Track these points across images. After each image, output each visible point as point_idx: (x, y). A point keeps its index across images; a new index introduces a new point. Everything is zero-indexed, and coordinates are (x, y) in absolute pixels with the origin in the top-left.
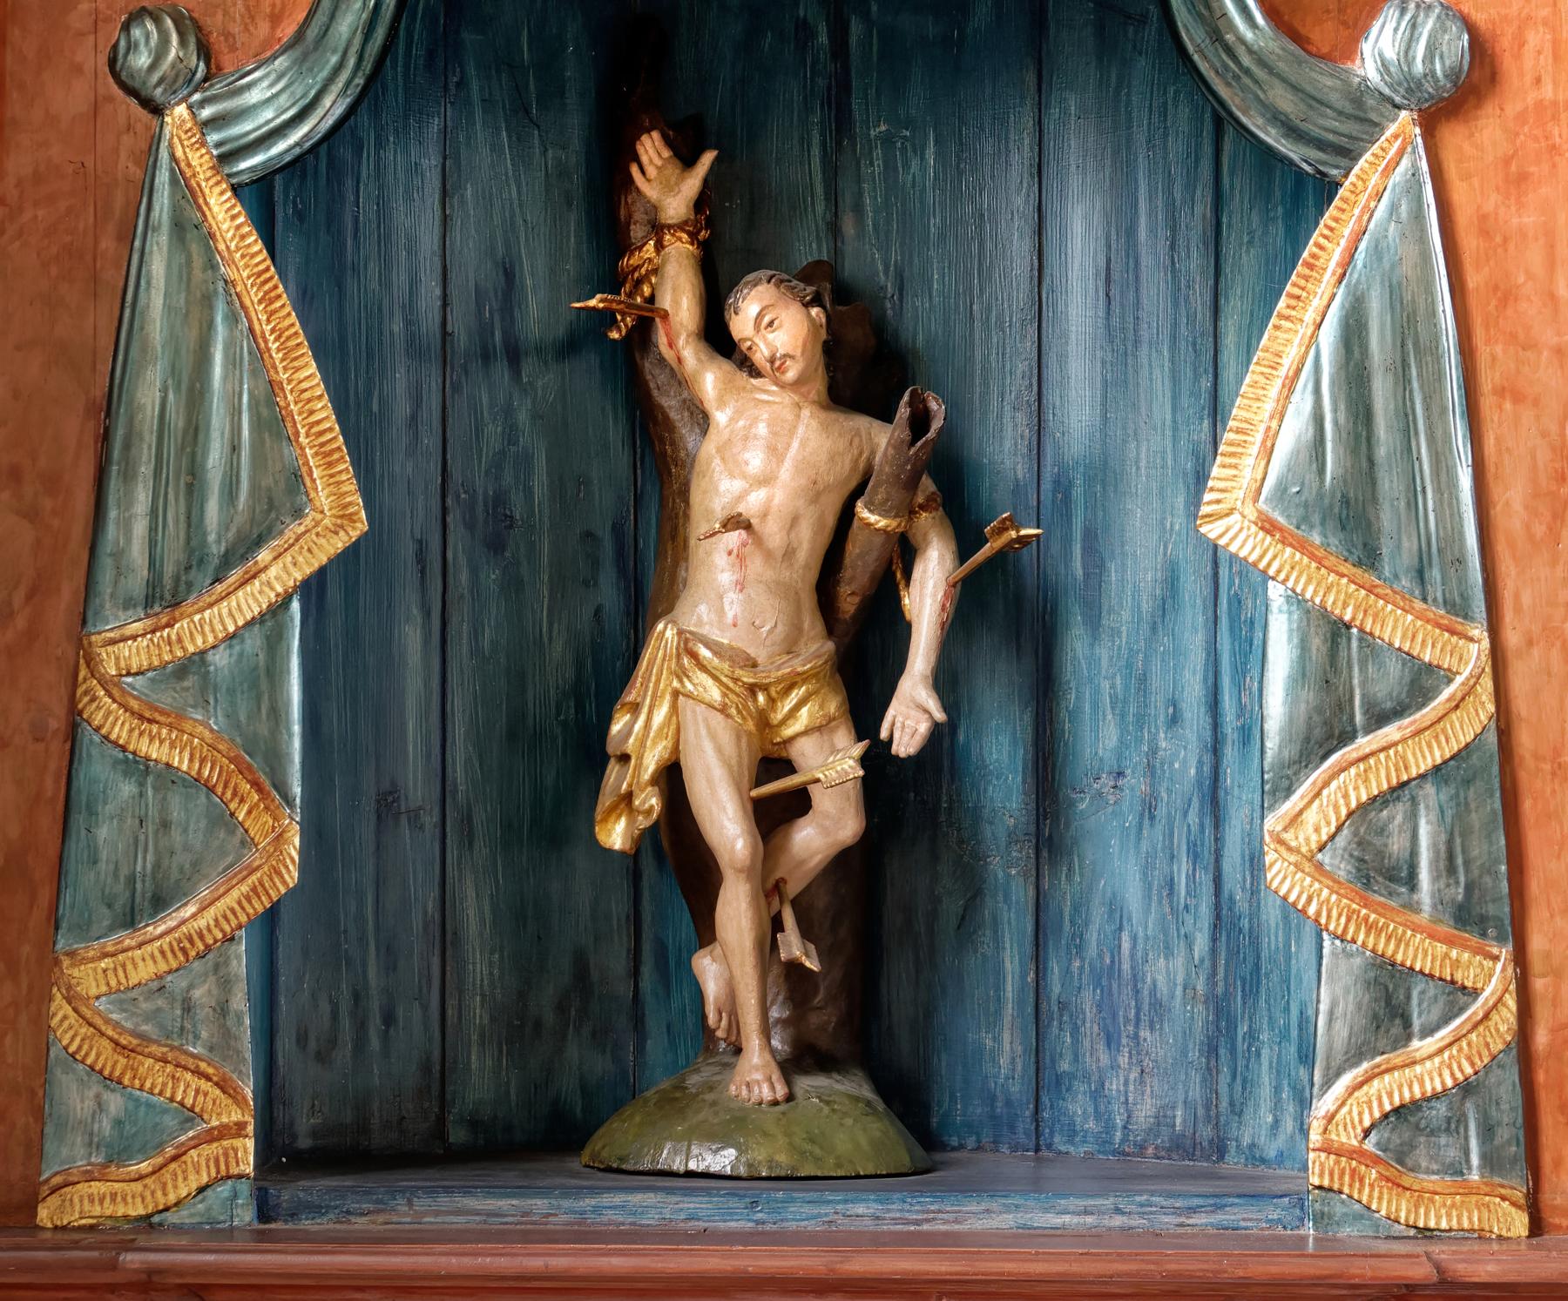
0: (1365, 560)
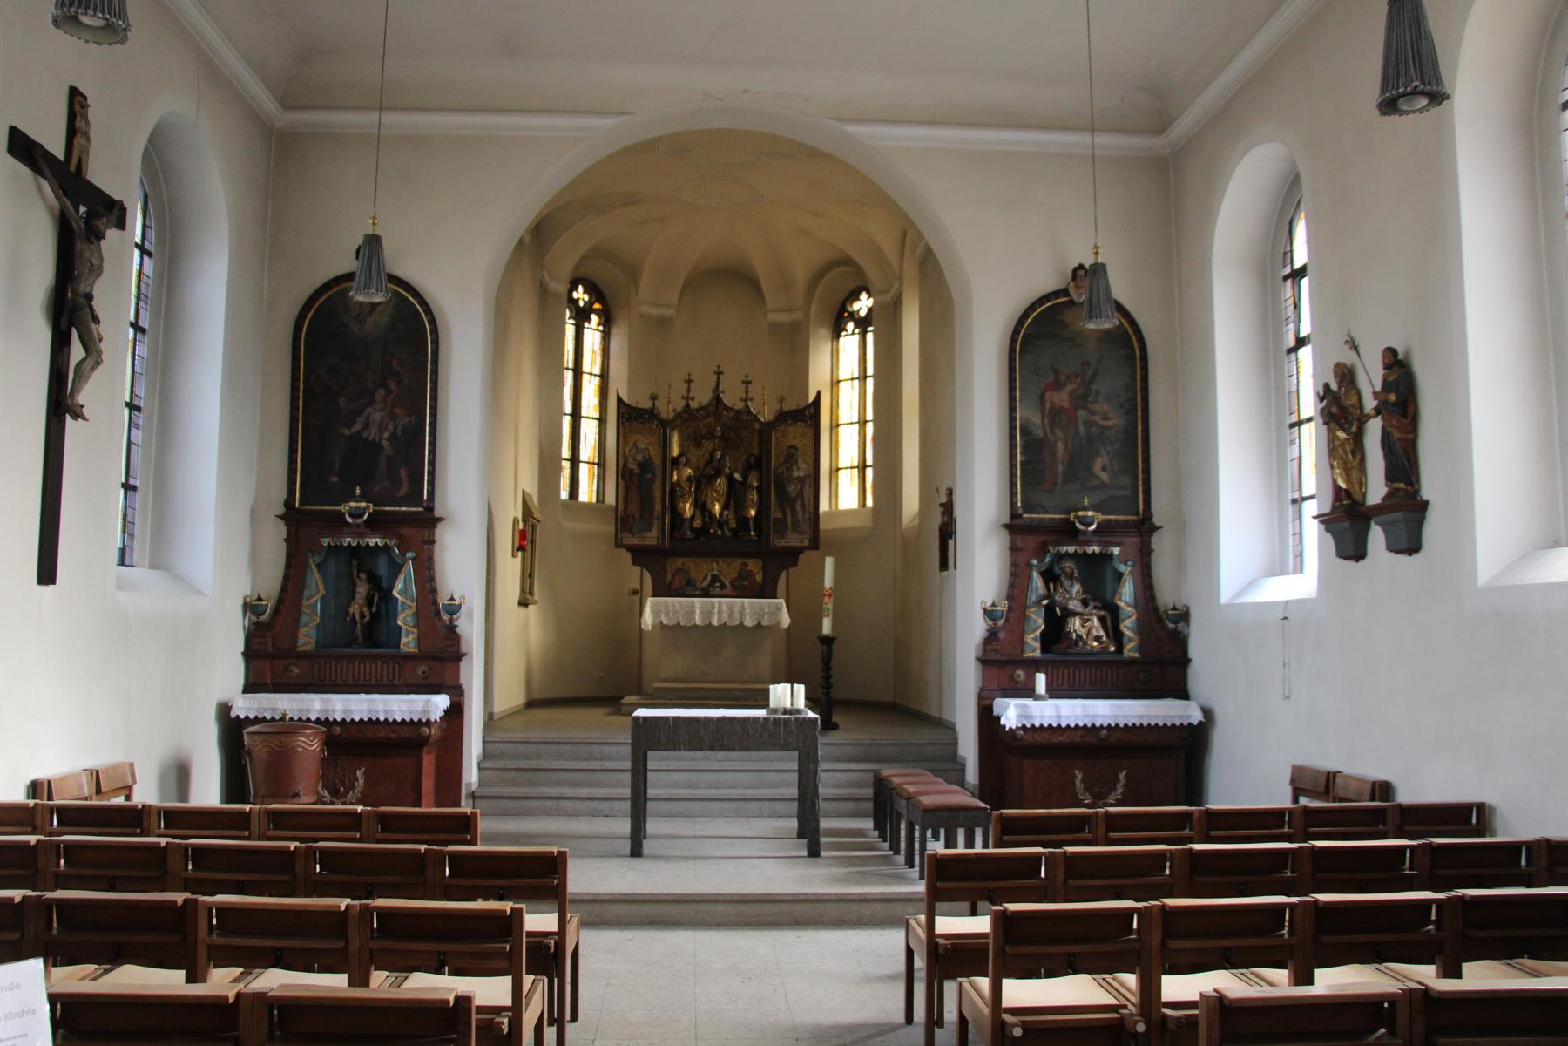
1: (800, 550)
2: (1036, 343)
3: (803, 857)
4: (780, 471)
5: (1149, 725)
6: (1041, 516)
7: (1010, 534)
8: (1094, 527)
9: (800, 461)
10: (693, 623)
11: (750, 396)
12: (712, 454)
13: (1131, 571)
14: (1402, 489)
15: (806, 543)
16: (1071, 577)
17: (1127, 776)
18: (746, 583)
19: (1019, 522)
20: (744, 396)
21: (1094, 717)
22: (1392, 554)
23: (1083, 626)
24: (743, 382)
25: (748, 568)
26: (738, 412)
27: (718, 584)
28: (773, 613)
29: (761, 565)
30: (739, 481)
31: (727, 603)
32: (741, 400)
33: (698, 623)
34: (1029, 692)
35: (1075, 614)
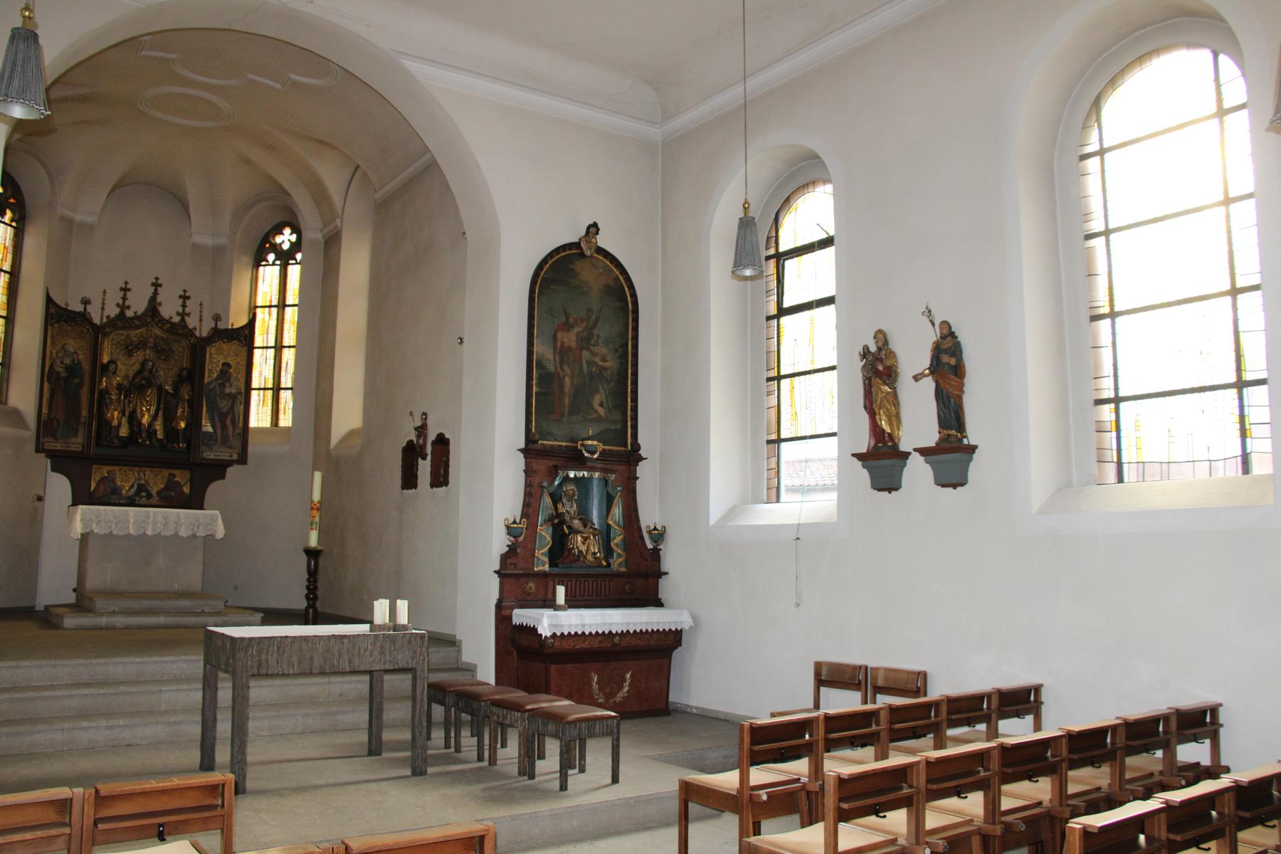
0: (531, 446)
1: (230, 463)
2: (552, 286)
3: (407, 777)
4: (211, 387)
5: (635, 631)
6: (551, 443)
7: (526, 457)
8: (596, 456)
9: (232, 379)
10: (126, 533)
11: (187, 310)
12: (144, 363)
13: (620, 495)
14: (954, 435)
15: (235, 457)
16: (570, 499)
17: (631, 676)
18: (173, 494)
19: (531, 446)
20: (180, 310)
21: (611, 624)
22: (939, 487)
23: (584, 543)
24: (180, 297)
25: (176, 479)
26: (174, 324)
27: (144, 494)
28: (208, 524)
29: (188, 476)
30: (171, 394)
31: (153, 512)
32: (178, 314)
33: (131, 532)
34: (549, 603)
35: (577, 532)
